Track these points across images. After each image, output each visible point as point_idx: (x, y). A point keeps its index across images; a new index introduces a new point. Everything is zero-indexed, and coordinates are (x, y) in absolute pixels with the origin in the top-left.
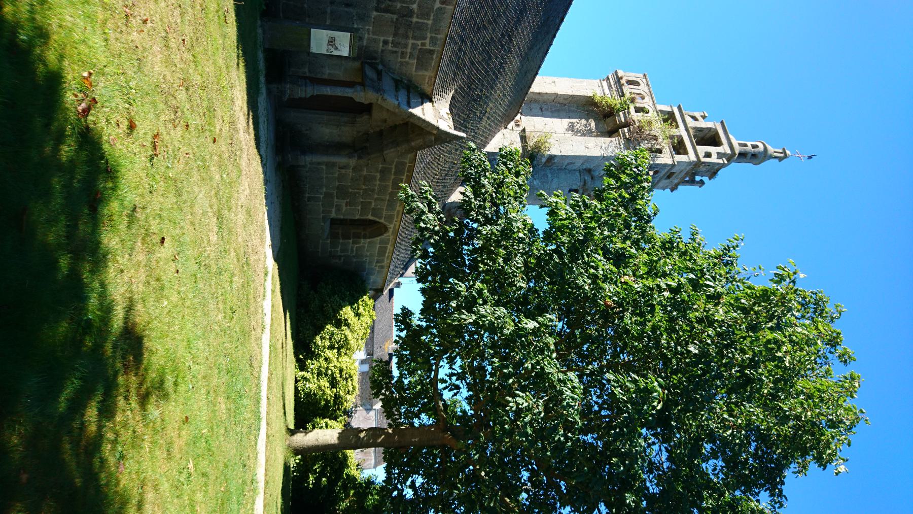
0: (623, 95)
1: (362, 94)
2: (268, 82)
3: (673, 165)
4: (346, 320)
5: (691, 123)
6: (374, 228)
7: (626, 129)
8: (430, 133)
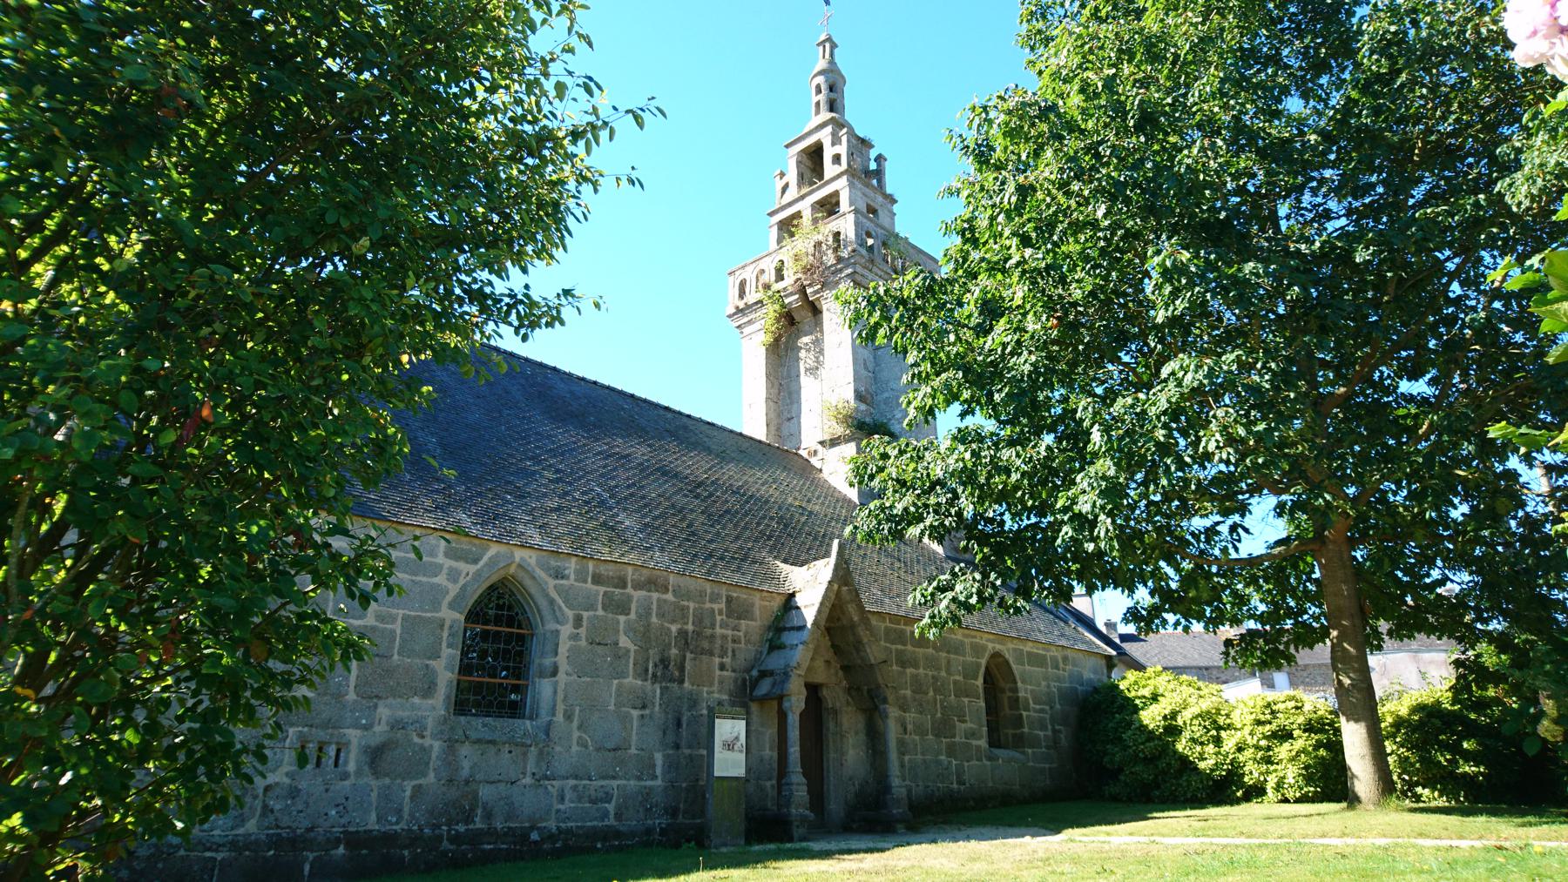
0: (761, 302)
1: (794, 699)
2: (791, 840)
3: (856, 211)
4: (1165, 718)
5: (793, 192)
6: (997, 678)
7: (809, 291)
8: (838, 592)
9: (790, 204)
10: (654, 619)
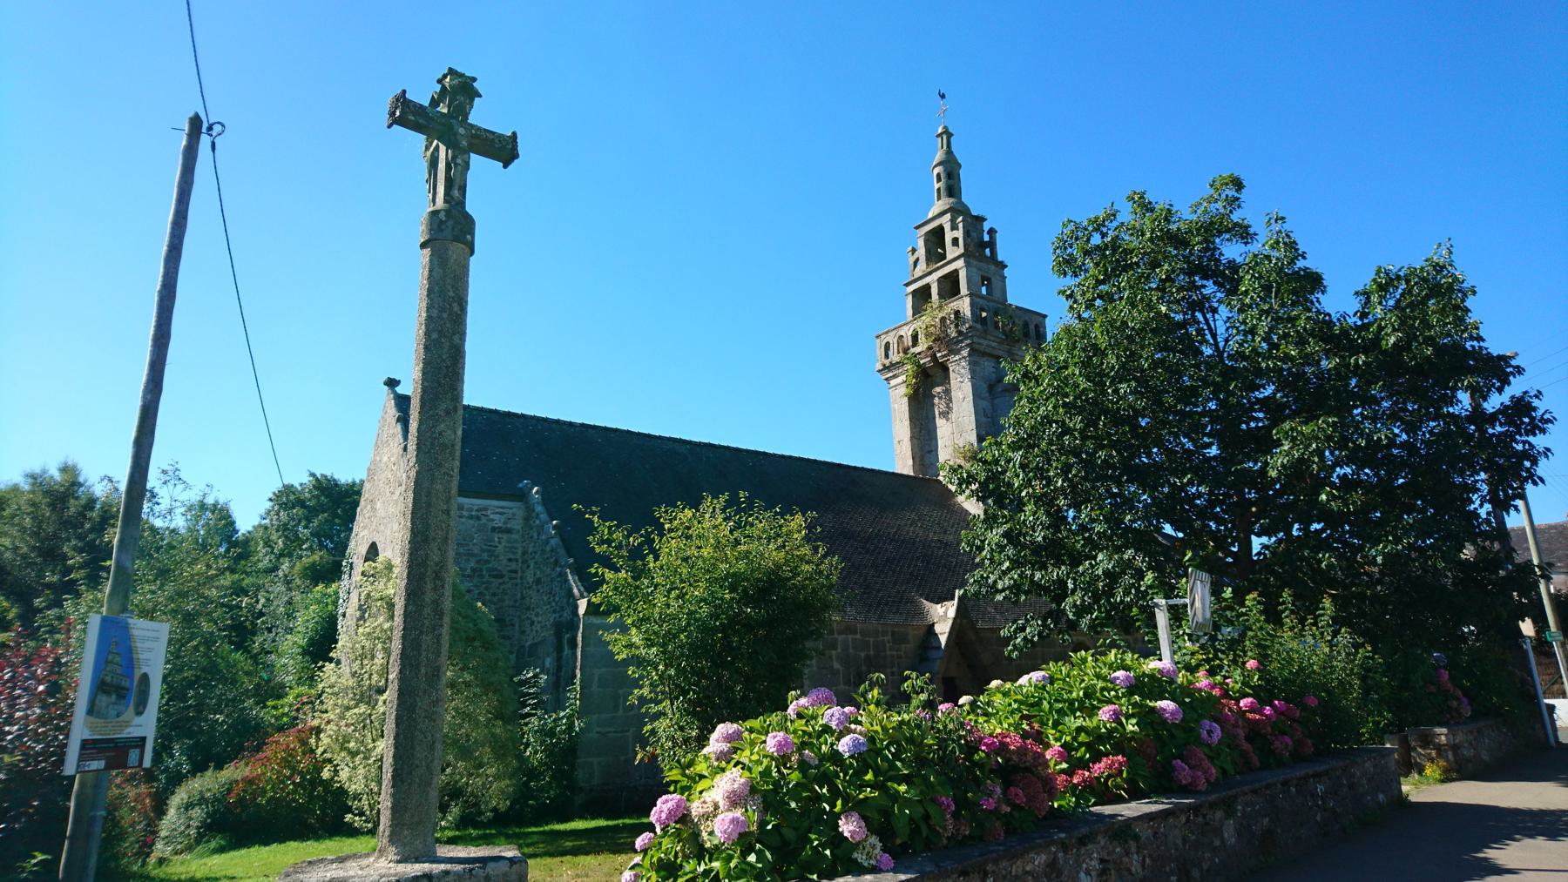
5: (922, 267)
9: (921, 278)
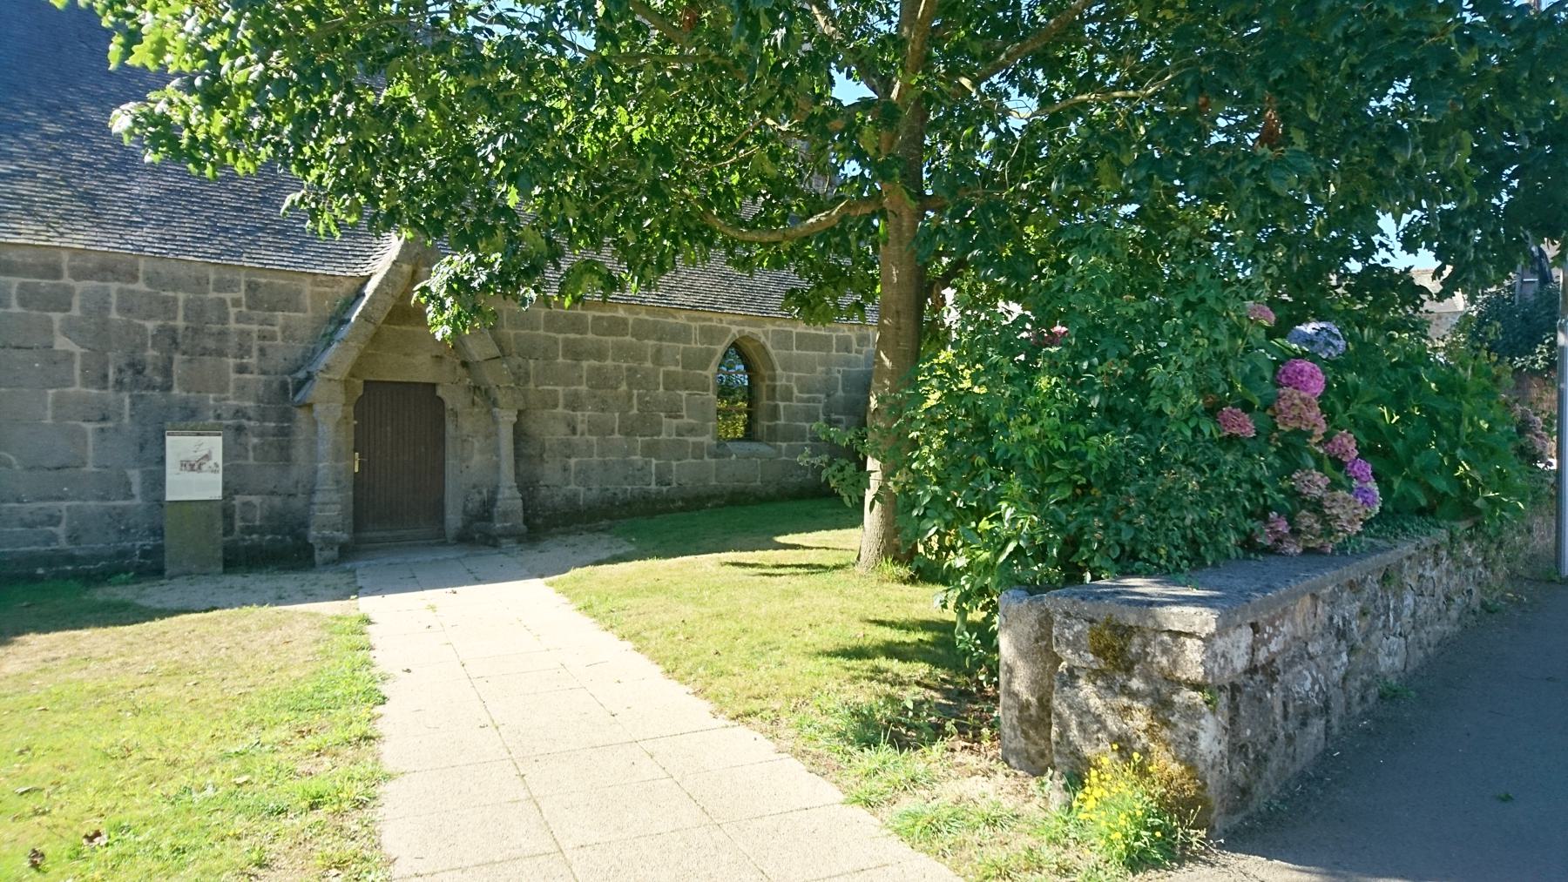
10: (114, 315)
